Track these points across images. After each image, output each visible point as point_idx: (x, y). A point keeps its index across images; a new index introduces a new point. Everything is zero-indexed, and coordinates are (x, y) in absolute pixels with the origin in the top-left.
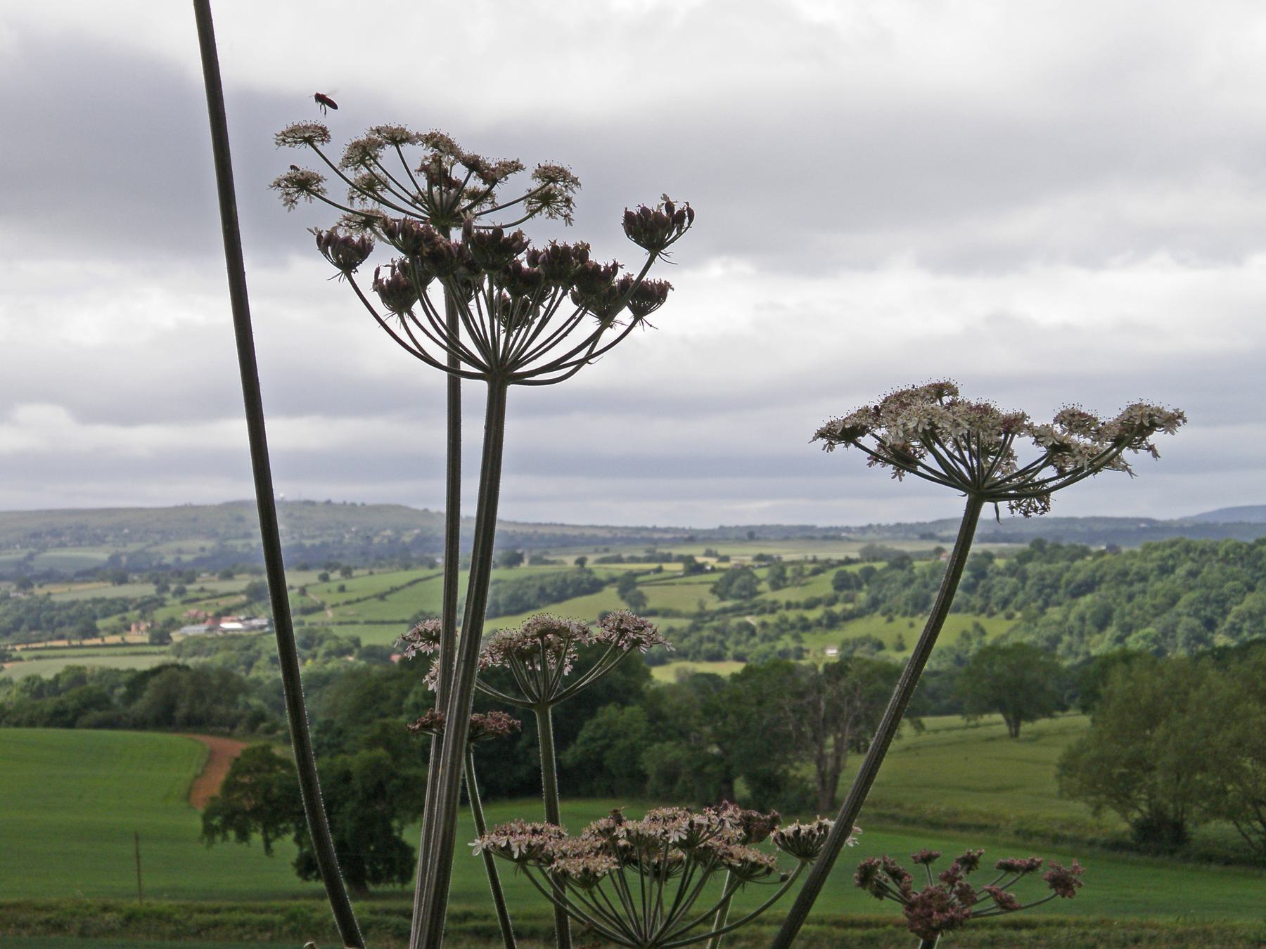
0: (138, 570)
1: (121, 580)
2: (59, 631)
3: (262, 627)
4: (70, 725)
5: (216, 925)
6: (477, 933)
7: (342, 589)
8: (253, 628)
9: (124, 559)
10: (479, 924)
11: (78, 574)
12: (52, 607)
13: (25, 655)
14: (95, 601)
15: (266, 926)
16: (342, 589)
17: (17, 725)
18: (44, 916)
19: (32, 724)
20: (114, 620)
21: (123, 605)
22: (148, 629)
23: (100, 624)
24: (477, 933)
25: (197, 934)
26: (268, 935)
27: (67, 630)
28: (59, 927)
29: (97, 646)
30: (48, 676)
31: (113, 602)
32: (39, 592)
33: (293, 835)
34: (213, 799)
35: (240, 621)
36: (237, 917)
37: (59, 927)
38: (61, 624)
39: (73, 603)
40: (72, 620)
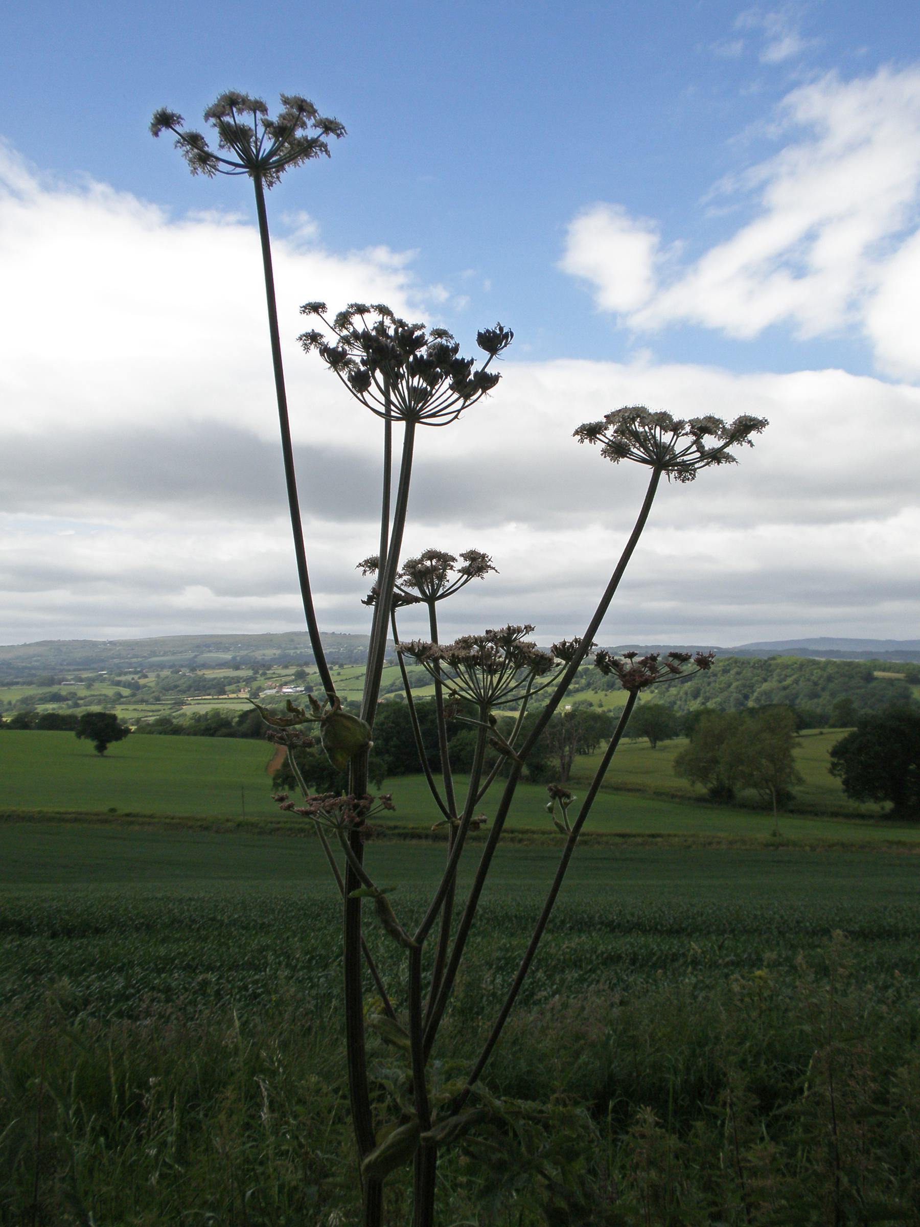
0: (244, 664)
1: (237, 668)
2: (208, 692)
3: (302, 691)
4: (213, 735)
5: (278, 829)
6: (400, 835)
7: (339, 674)
8: (297, 692)
9: (238, 658)
10: (401, 831)
11: (217, 665)
12: (205, 680)
13: (192, 702)
14: (225, 678)
15: (302, 830)
16: (339, 674)
17: (188, 734)
18: (199, 823)
19: (195, 734)
20: (233, 687)
21: (238, 680)
22: (249, 691)
23: (227, 688)
24: (400, 835)
25: (270, 833)
26: (303, 835)
27: (212, 691)
28: (206, 828)
29: (225, 699)
30: (203, 712)
31: (233, 678)
32: (200, 673)
33: (315, 788)
34: (278, 771)
35: (291, 688)
36: (288, 825)
37: (206, 828)
38: (209, 688)
39: (215, 679)
40: (214, 686)
